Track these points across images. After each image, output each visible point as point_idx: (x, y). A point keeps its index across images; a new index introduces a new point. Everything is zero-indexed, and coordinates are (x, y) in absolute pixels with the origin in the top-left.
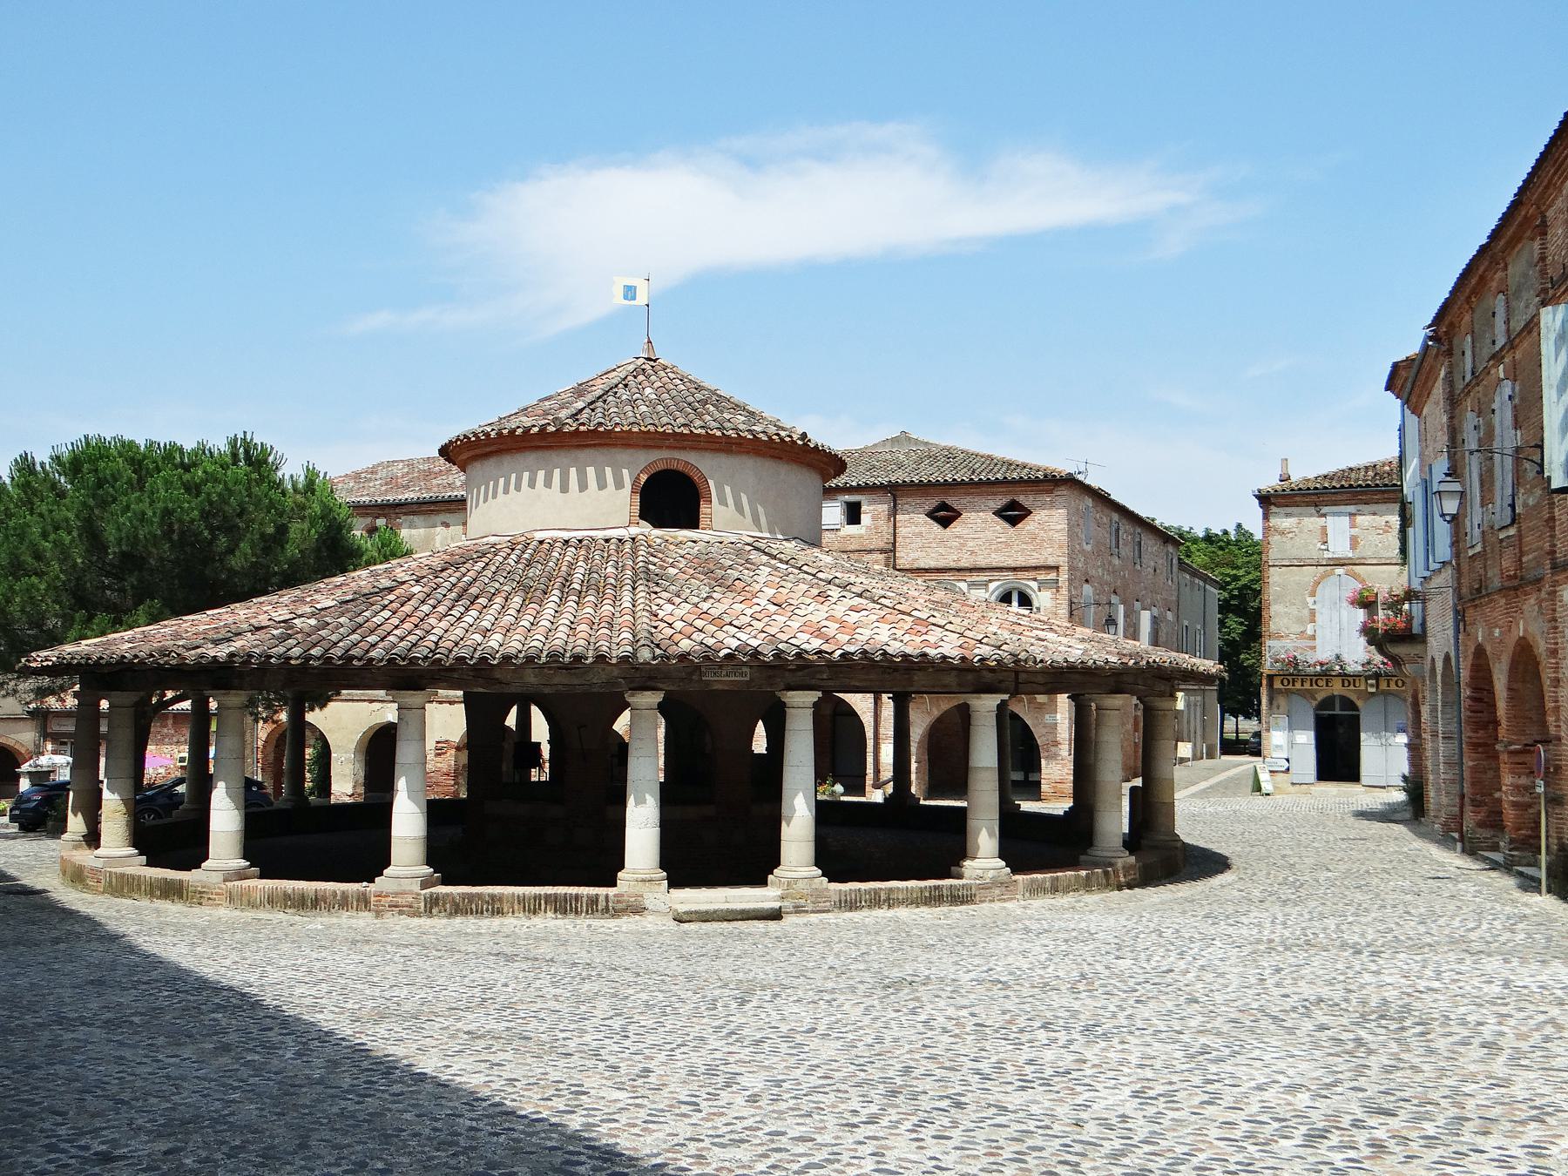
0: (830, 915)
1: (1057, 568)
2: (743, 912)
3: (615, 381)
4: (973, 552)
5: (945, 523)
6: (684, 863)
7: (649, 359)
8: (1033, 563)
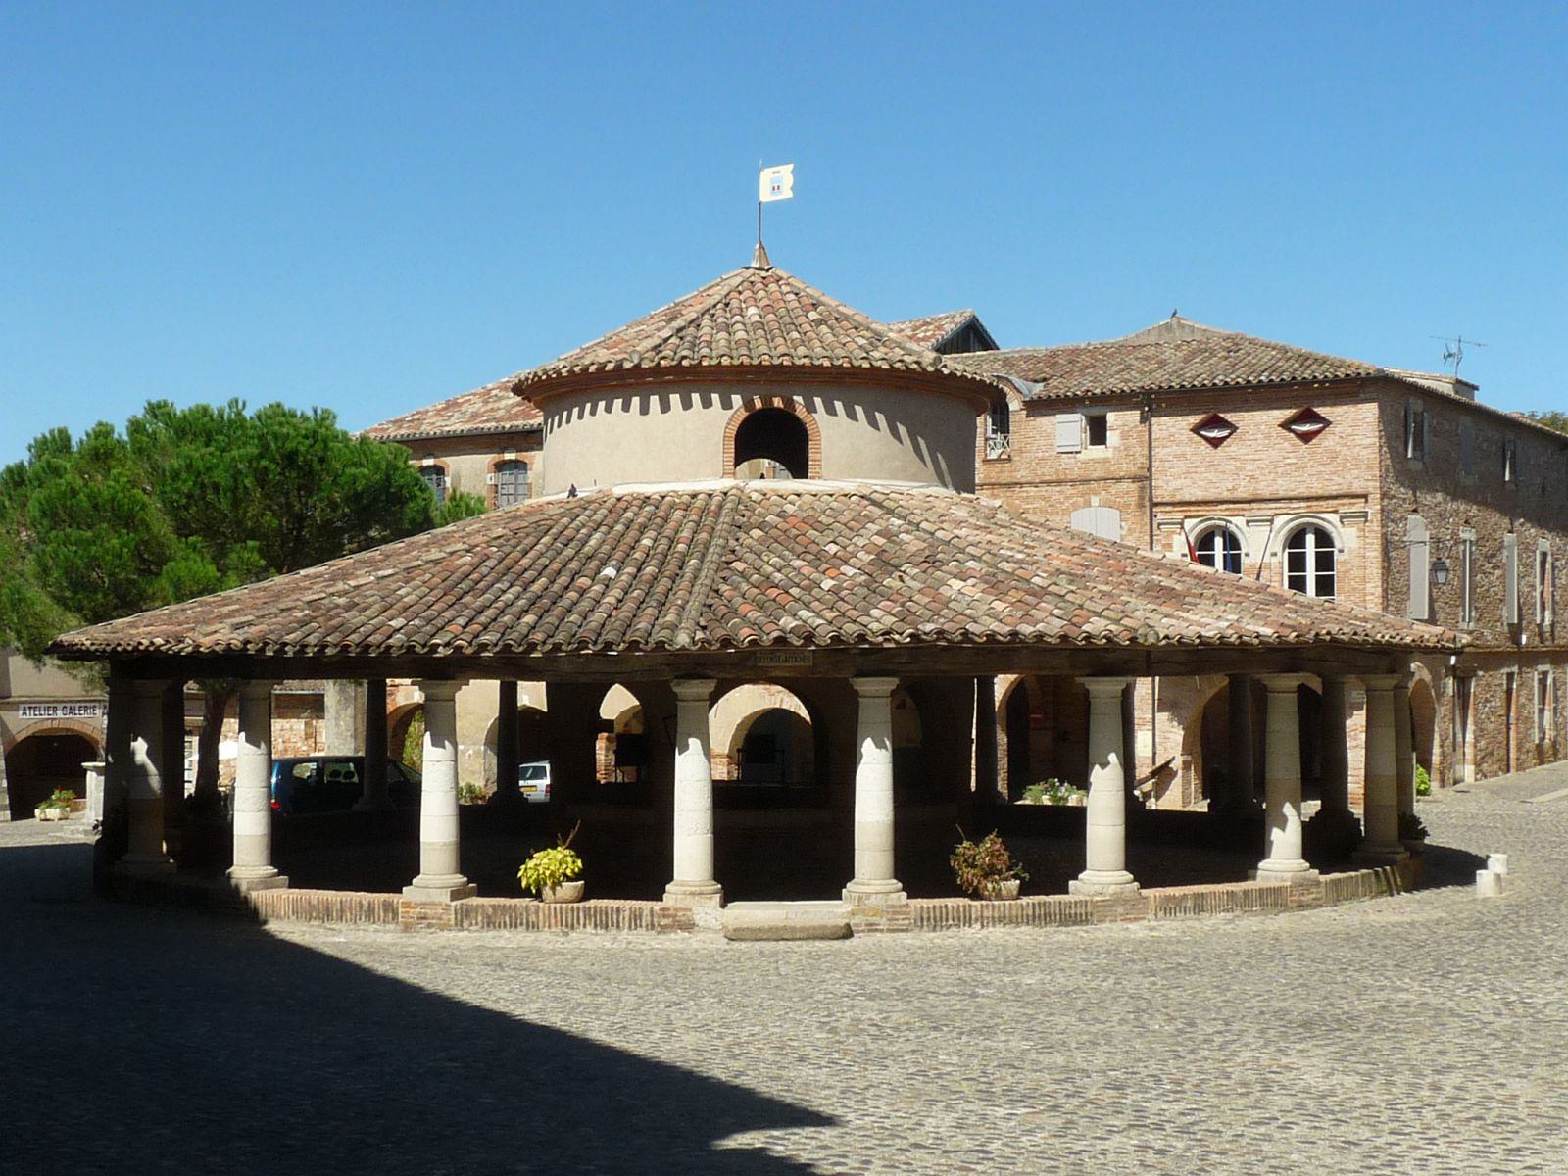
1: (1365, 496)
3: (713, 301)
4: (1252, 477)
6: (741, 872)
7: (761, 269)
8: (1333, 490)
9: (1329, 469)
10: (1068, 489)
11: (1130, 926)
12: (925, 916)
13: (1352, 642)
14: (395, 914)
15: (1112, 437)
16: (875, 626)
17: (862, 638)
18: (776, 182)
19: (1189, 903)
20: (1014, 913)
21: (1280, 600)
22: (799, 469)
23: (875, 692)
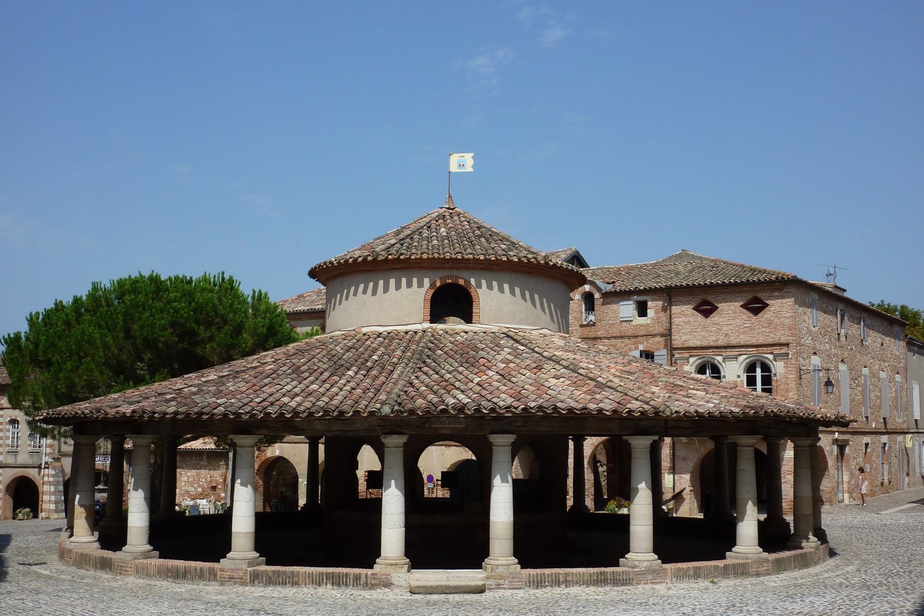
0: (522, 591)
2: (456, 587)
3: (421, 225)
4: (726, 335)
5: (707, 313)
6: (420, 553)
9: (768, 330)
10: (627, 341)
11: (655, 586)
12: (532, 579)
13: (786, 416)
14: (215, 575)
15: (650, 313)
16: (501, 404)
17: (493, 410)
18: (462, 162)
19: (691, 573)
20: (586, 578)
21: (745, 395)
22: (468, 319)
23: (502, 442)
